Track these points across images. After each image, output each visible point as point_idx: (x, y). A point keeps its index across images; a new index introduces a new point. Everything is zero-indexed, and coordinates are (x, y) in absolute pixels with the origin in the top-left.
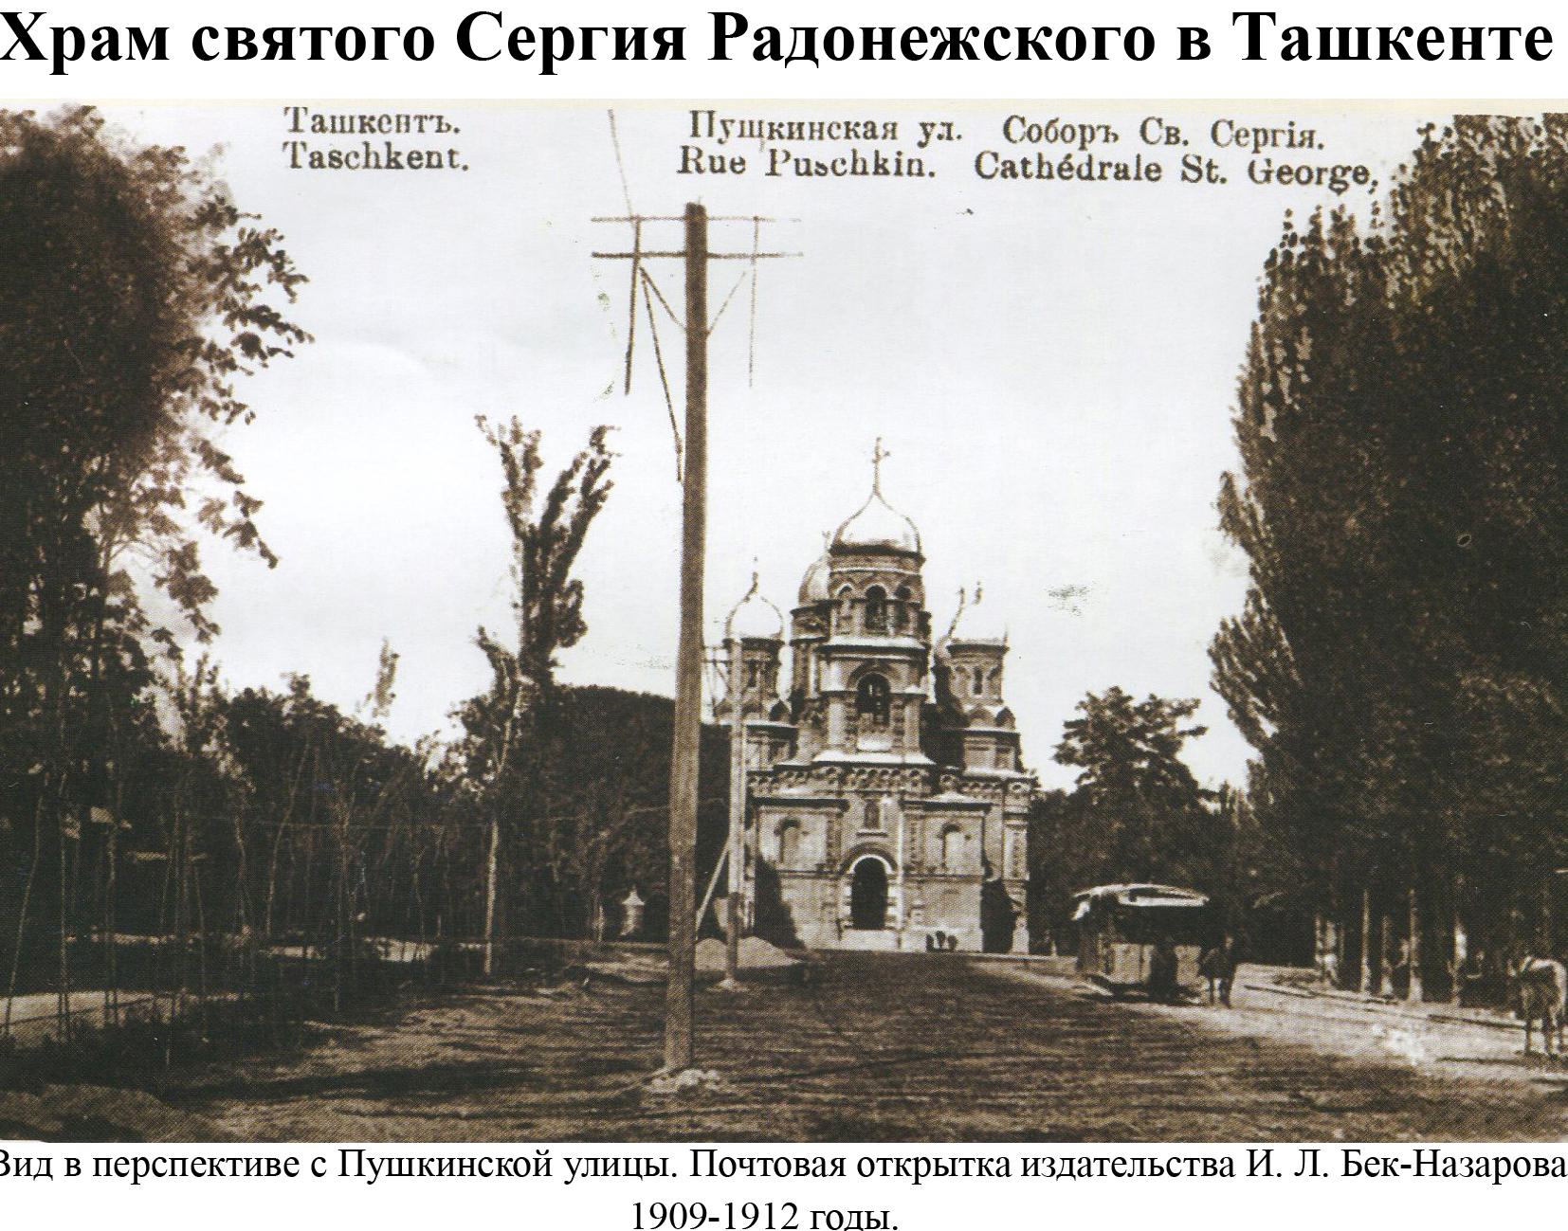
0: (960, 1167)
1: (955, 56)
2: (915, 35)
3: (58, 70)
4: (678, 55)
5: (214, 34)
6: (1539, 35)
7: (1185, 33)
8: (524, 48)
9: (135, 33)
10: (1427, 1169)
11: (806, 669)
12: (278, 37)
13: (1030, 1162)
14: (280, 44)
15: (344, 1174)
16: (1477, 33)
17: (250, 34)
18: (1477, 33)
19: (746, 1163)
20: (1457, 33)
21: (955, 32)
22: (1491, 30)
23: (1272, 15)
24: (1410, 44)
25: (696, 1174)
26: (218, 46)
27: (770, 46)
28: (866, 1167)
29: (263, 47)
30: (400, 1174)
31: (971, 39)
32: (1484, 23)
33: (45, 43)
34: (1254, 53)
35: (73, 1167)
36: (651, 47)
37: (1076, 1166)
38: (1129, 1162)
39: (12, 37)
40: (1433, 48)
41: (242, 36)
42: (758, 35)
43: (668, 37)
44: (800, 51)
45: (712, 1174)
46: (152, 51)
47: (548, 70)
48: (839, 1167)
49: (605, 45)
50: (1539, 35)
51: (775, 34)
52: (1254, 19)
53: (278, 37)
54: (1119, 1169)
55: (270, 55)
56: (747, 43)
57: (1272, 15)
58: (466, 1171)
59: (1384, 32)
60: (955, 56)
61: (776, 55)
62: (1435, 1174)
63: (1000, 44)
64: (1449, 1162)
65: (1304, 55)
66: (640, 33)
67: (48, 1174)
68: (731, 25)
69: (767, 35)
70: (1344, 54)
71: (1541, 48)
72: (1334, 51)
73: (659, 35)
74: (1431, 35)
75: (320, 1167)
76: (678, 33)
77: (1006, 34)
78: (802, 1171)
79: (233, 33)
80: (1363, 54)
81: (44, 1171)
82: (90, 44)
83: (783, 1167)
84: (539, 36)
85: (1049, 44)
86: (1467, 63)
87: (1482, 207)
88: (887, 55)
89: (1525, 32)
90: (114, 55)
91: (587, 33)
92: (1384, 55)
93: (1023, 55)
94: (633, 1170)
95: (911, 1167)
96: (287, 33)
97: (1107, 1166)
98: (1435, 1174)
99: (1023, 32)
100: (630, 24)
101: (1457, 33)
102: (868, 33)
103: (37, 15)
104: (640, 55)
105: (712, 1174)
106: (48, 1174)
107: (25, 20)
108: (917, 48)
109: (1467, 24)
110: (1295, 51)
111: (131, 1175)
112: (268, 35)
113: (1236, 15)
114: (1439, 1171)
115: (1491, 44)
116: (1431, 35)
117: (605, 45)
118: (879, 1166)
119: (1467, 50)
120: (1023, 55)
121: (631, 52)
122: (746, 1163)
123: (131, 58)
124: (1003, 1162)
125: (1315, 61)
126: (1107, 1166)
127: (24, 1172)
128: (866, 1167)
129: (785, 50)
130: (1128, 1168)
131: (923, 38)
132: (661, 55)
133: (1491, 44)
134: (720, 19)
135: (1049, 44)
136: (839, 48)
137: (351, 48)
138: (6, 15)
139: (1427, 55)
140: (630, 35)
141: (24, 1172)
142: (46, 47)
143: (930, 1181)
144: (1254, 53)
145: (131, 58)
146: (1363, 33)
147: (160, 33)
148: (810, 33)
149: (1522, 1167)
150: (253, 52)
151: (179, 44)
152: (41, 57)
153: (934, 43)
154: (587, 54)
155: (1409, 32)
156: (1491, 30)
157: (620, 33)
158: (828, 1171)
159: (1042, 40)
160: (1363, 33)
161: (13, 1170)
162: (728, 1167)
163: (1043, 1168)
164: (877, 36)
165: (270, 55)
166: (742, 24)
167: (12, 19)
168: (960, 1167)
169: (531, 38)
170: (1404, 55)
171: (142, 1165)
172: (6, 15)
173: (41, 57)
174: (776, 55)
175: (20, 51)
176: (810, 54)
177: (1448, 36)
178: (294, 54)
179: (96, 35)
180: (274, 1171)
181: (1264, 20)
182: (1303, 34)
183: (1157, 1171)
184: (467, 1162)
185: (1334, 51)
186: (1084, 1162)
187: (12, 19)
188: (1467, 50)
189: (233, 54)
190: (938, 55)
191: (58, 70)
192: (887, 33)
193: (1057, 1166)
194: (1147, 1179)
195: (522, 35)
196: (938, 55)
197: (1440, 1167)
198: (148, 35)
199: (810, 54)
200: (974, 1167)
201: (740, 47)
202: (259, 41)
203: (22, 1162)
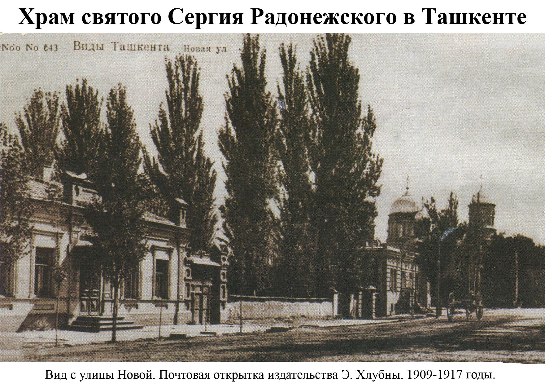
0: (247, 376)
1: (331, 23)
2: (318, 16)
4: (241, 22)
5: (89, 15)
6: (522, 16)
7: (406, 15)
8: (190, 20)
9: (63, 15)
10: (122, 376)
12: (110, 16)
13: (271, 374)
14: (111, 19)
15: (161, 378)
16: (502, 15)
17: (101, 15)
18: (502, 15)
19: (178, 374)
20: (495, 15)
21: (331, 15)
22: (506, 14)
23: (435, 9)
24: (480, 19)
25: (161, 378)
26: (90, 19)
27: (271, 19)
28: (217, 376)
29: (105, 20)
31: (336, 17)
32: (504, 12)
33: (34, 19)
34: (429, 22)
36: (232, 20)
37: (286, 376)
38: (303, 374)
39: (23, 16)
40: (487, 20)
41: (98, 16)
43: (238, 16)
44: (281, 21)
45: (166, 378)
46: (69, 21)
48: (208, 376)
49: (217, 19)
50: (522, 16)
51: (272, 15)
52: (429, 11)
53: (110, 16)
54: (300, 376)
55: (108, 22)
56: (263, 18)
57: (435, 9)
59: (471, 15)
60: (331, 23)
61: (273, 22)
62: (125, 378)
63: (346, 19)
65: (445, 22)
66: (228, 15)
67: (65, 378)
68: (258, 13)
69: (270, 16)
70: (458, 22)
71: (523, 20)
72: (455, 21)
73: (234, 16)
74: (487, 16)
75: (73, 376)
76: (241, 15)
77: (348, 15)
78: (196, 377)
79: (95, 15)
80: (464, 22)
81: (64, 377)
82: (49, 19)
83: (189, 376)
84: (195, 16)
85: (362, 19)
86: (498, 25)
88: (309, 22)
89: (517, 15)
90: (56, 22)
91: (211, 15)
92: (471, 22)
93: (353, 22)
94: (102, 377)
95: (231, 376)
96: (113, 15)
98: (125, 378)
99: (353, 15)
100: (225, 12)
102: (303, 15)
103: (31, 9)
104: (228, 22)
105: (166, 378)
106: (65, 378)
107: (27, 11)
108: (319, 20)
109: (498, 12)
110: (442, 21)
112: (107, 16)
113: (423, 9)
115: (506, 19)
116: (487, 16)
118: (221, 375)
119: (498, 21)
120: (353, 22)
121: (225, 21)
122: (178, 374)
124: (261, 374)
125: (449, 25)
127: (57, 377)
128: (217, 376)
129: (276, 21)
130: (303, 376)
131: (321, 17)
132: (235, 22)
133: (506, 19)
134: (254, 10)
135: (362, 19)
136: (293, 20)
137: (134, 20)
138: (21, 9)
139: (485, 22)
141: (57, 377)
142: (34, 20)
143: (237, 380)
144: (429, 22)
146: (464, 15)
147: (72, 15)
148: (284, 15)
150: (102, 21)
153: (324, 18)
154: (211, 22)
155: (479, 15)
156: (506, 14)
157: (222, 15)
158: (204, 377)
160: (464, 15)
162: (171, 376)
163: (275, 376)
165: (108, 22)
166: (262, 12)
167: (23, 10)
168: (247, 376)
169: (193, 17)
170: (478, 22)
172: (21, 9)
174: (273, 22)
175: (26, 21)
176: (284, 22)
177: (492, 16)
179: (51, 16)
181: (432, 11)
182: (445, 15)
183: (312, 377)
185: (455, 21)
186: (289, 374)
187: (23, 10)
188: (498, 21)
189: (95, 22)
190: (326, 22)
192: (309, 15)
193: (280, 376)
194: (309, 380)
195: (190, 16)
196: (326, 22)
198: (67, 16)
199: (284, 22)
200: (252, 376)
202: (104, 18)
203: (57, 374)
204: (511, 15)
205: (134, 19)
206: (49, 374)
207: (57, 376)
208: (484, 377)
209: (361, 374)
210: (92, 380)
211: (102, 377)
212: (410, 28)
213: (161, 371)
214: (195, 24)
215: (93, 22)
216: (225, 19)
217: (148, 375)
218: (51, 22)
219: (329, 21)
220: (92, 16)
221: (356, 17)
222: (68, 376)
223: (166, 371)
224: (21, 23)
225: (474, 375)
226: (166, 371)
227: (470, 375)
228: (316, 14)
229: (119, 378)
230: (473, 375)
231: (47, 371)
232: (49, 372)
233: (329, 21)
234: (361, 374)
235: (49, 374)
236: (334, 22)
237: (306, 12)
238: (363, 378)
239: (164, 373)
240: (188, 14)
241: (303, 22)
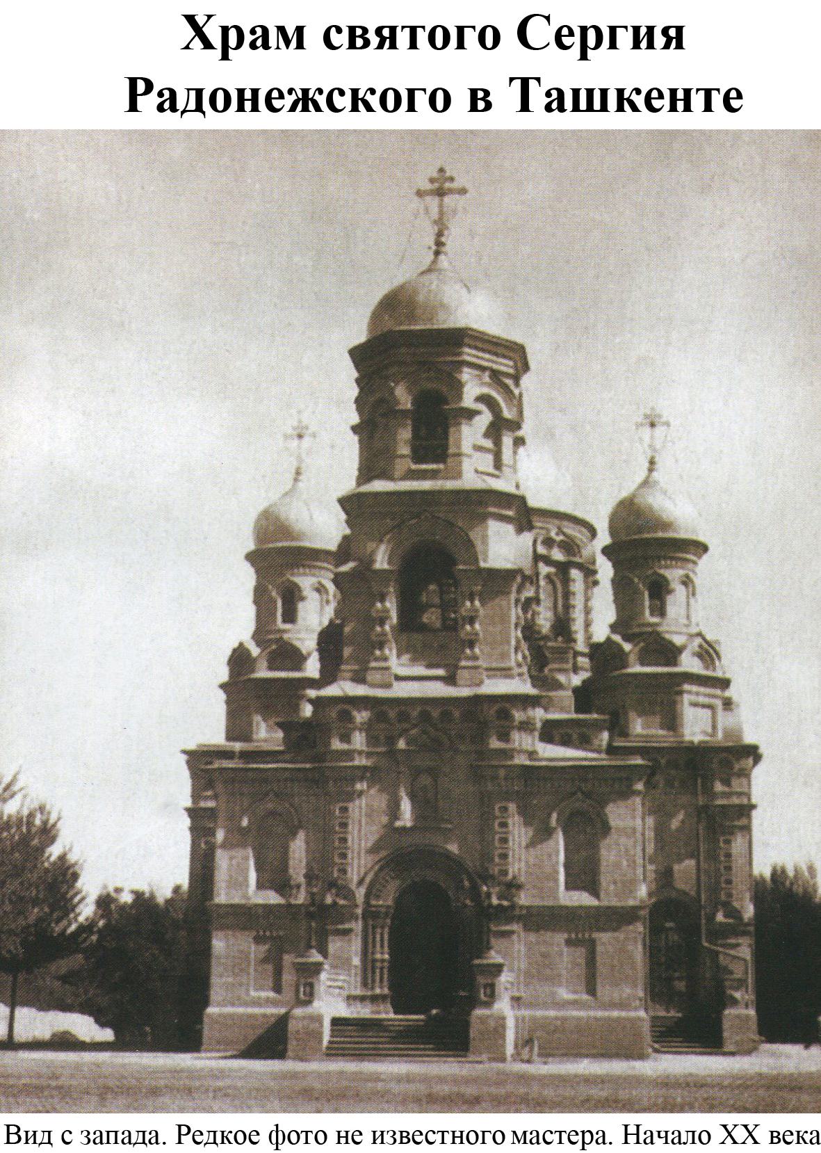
1: (305, 109)
2: (275, 94)
3: (225, 57)
4: (680, 46)
5: (339, 30)
6: (733, 94)
7: (474, 92)
8: (566, 41)
9: (281, 30)
10: (632, 1139)
11: (567, 594)
12: (386, 33)
13: (378, 1134)
14: (388, 38)
16: (687, 92)
17: (365, 30)
18: (687, 92)
19: (663, 1134)
20: (673, 92)
21: (305, 91)
22: (698, 90)
23: (538, 79)
24: (639, 101)
26: (340, 39)
27: (169, 102)
29: (375, 40)
31: (317, 97)
33: (215, 37)
34: (525, 107)
35: (182, 1131)
36: (659, 40)
37: (148, 1137)
38: (206, 1134)
39: (191, 33)
40: (656, 104)
41: (359, 32)
42: (160, 94)
43: (672, 33)
44: (192, 105)
46: (294, 43)
47: (584, 57)
49: (625, 38)
50: (733, 94)
51: (173, 93)
52: (525, 82)
53: (386, 33)
54: (198, 1139)
55: (380, 46)
57: (538, 79)
58: (457, 1140)
59: (620, 92)
60: (305, 109)
61: (173, 108)
62: (638, 1142)
64: (649, 1134)
65: (561, 108)
66: (650, 30)
67: (49, 1142)
68: (141, 87)
69: (167, 94)
70: (590, 108)
71: (735, 104)
73: (665, 31)
74: (655, 94)
75: (68, 1137)
76: (679, 30)
77: (342, 93)
79: (352, 29)
80: (604, 108)
81: (46, 1140)
82: (248, 38)
84: (577, 32)
85: (374, 101)
87: (296, 259)
88: (255, 108)
89: (723, 92)
90: (266, 46)
91: (613, 30)
92: (620, 108)
93: (355, 108)
94: (112, 1135)
96: (393, 30)
97: (565, 1136)
98: (638, 1142)
99: (355, 92)
100: (643, 23)
101: (673, 92)
102: (241, 92)
103: (209, 17)
104: (650, 46)
106: (49, 1142)
107: (200, 20)
108: (277, 104)
109: (680, 85)
111: (580, 1143)
112: (379, 31)
113: (511, 79)
114: (641, 1140)
115: (698, 100)
116: (655, 94)
117: (625, 38)
118: (303, 1136)
119: (680, 105)
120: (355, 108)
121: (644, 44)
122: (663, 1134)
123: (278, 48)
126: (565, 1136)
127: (31, 1141)
129: (180, 105)
130: (204, 1138)
131: (281, 96)
132: (667, 46)
133: (698, 100)
134: (133, 82)
135: (374, 101)
136: (220, 103)
137: (439, 41)
138: (186, 16)
139: (651, 109)
140: (643, 31)
141: (31, 1141)
142: (216, 40)
144: (525, 107)
145: (278, 48)
146: (604, 92)
147: (300, 30)
148: (199, 92)
149: (240, 1137)
150: (367, 43)
151: (313, 37)
152: (212, 47)
153: (289, 100)
154: (613, 45)
155: (638, 91)
157: (636, 30)
159: (369, 97)
161: (23, 1140)
165: (380, 46)
166: (149, 86)
167: (191, 19)
169: (571, 34)
170: (634, 108)
171: (588, 1136)
172: (186, 16)
173: (212, 47)
174: (173, 108)
175: (197, 43)
176: (199, 108)
177: (667, 95)
178: (398, 45)
179: (253, 32)
180: (405, 1140)
181: (532, 83)
182: (561, 93)
184: (458, 1134)
187: (191, 19)
188: (680, 105)
189: (352, 46)
190: (293, 109)
191: (225, 57)
192: (255, 92)
193: (92, 1137)
195: (565, 31)
196: (293, 109)
197: (642, 1137)
198: (290, 31)
199: (199, 108)
202: (371, 36)
203: (30, 1134)
204: (708, 93)
205: (441, 38)
206: (14, 1134)
207: (31, 1137)
208: (219, 1140)
209: (729, 1134)
211: (112, 1135)
212: (480, 121)
214: (576, 50)
215: (346, 44)
216: (643, 38)
217: (250, 1138)
220: (346, 31)
221: (360, 96)
222: (56, 1138)
224: (187, 47)
228: (272, 90)
229: (626, 1142)
230: (521, 1138)
234: (729, 1134)
235: (14, 1134)
236: (311, 107)
237: (248, 85)
238: (735, 1142)
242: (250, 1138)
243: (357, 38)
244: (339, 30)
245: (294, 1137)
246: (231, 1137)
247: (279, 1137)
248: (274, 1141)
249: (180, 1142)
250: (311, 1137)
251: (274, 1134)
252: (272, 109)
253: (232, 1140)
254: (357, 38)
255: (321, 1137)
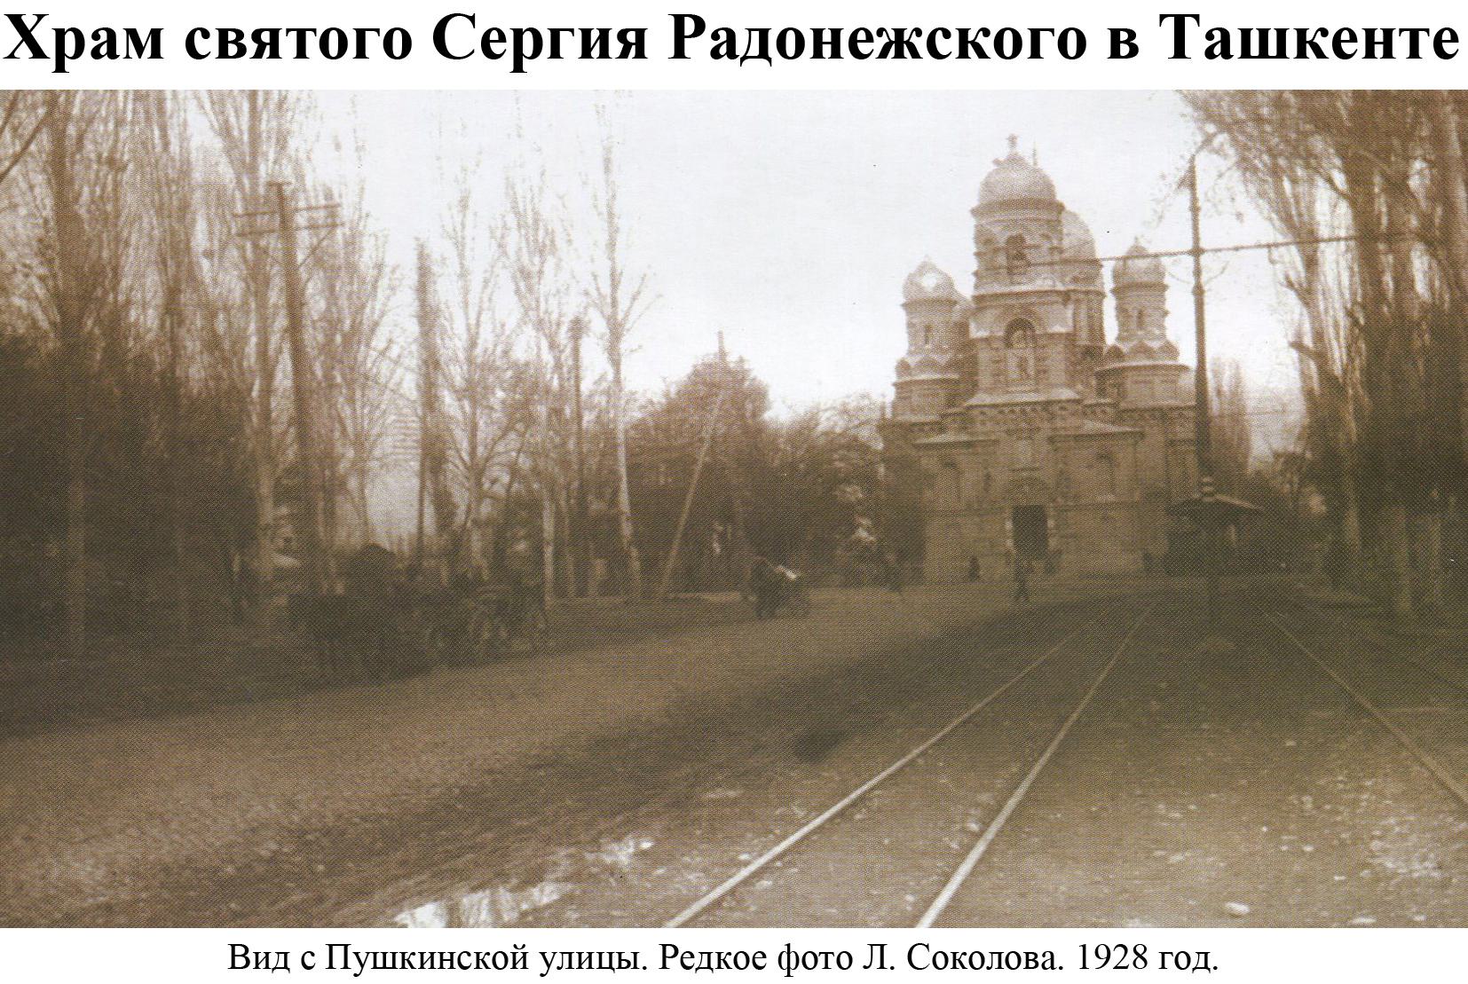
1: (899, 55)
2: (862, 36)
4: (640, 54)
5: (206, 34)
6: (1446, 36)
7: (1115, 33)
8: (496, 48)
9: (132, 33)
12: (266, 37)
13: (520, 965)
14: (268, 44)
15: (331, 967)
16: (1388, 33)
17: (240, 34)
18: (1388, 33)
20: (1370, 33)
21: (899, 32)
22: (1401, 30)
23: (1197, 17)
24: (1326, 44)
25: (331, 967)
26: (208, 46)
27: (726, 46)
29: (252, 48)
30: (384, 967)
31: (914, 39)
32: (1396, 25)
34: (1180, 52)
36: (615, 47)
38: (698, 956)
40: (1347, 48)
41: (232, 36)
42: (715, 36)
43: (631, 37)
44: (755, 50)
46: (148, 51)
47: (518, 68)
50: (1446, 36)
52: (1180, 21)
53: (266, 37)
54: (688, 962)
55: (258, 55)
56: (705, 43)
57: (1197, 17)
59: (1301, 33)
60: (899, 55)
61: (731, 54)
63: (941, 44)
65: (1226, 54)
66: (604, 33)
67: (286, 967)
68: (689, 26)
69: (723, 36)
70: (1263, 53)
72: (1255, 49)
73: (622, 35)
74: (1345, 36)
75: (309, 961)
76: (640, 33)
77: (947, 34)
78: (1032, 964)
79: (223, 33)
80: (1281, 53)
81: (281, 964)
82: (90, 44)
84: (510, 36)
85: (987, 44)
88: (836, 54)
89: (1433, 33)
90: (112, 54)
91: (555, 33)
92: (1301, 54)
93: (963, 54)
94: (606, 963)
96: (274, 33)
99: (963, 33)
100: (595, 25)
101: (1370, 33)
102: (818, 33)
103: (40, 17)
104: (604, 54)
106: (286, 967)
107: (29, 21)
108: (863, 48)
109: (1379, 25)
110: (1217, 50)
112: (256, 35)
113: (1162, 17)
115: (1401, 44)
116: (1345, 36)
118: (821, 959)
119: (1379, 50)
121: (596, 52)
123: (128, 57)
127: (263, 965)
129: (740, 50)
130: (696, 961)
131: (869, 39)
132: (624, 55)
133: (1401, 44)
134: (679, 20)
135: (987, 44)
138: (11, 17)
141: (263, 965)
142: (48, 46)
144: (1180, 52)
146: (1281, 33)
147: (155, 34)
148: (764, 33)
149: (742, 961)
150: (242, 51)
151: (173, 44)
152: (44, 56)
153: (879, 43)
154: (555, 53)
155: (1324, 32)
156: (1401, 30)
157: (586, 33)
160: (1281, 33)
161: (253, 964)
164: (827, 37)
165: (258, 55)
166: (700, 25)
167: (16, 20)
169: (502, 38)
170: (1319, 54)
172: (11, 17)
173: (44, 56)
174: (731, 54)
175: (25, 51)
176: (763, 53)
177: (1361, 37)
179: (96, 36)
181: (1189, 22)
182: (1225, 35)
184: (446, 956)
185: (1255, 49)
187: (16, 20)
188: (1379, 50)
189: (223, 53)
190: (883, 54)
192: (836, 33)
195: (494, 36)
196: (883, 54)
198: (143, 36)
199: (763, 53)
201: (698, 47)
202: (248, 41)
203: (261, 956)
206: (240, 957)
208: (714, 964)
210: (575, 972)
213: (331, 946)
214: (509, 59)
215: (216, 52)
217: (754, 961)
218: (96, 54)
219: (892, 52)
220: (215, 36)
221: (970, 38)
222: (294, 962)
223: (346, 946)
224: (12, 56)
225: (1183, 960)
226: (346, 946)
227: (1169, 960)
231: (233, 946)
232: (240, 950)
233: (892, 52)
236: (906, 52)
237: (827, 25)
239: (338, 953)
240: (489, 31)
241: (818, 54)
242: (754, 961)
243: (229, 43)
244: (206, 34)
245: (810, 960)
246: (730, 960)
247: (791, 961)
248: (785, 965)
249: (664, 967)
250: (832, 960)
251: (785, 956)
252: (857, 54)
253: (731, 964)
254: (229, 43)
255: (845, 960)
